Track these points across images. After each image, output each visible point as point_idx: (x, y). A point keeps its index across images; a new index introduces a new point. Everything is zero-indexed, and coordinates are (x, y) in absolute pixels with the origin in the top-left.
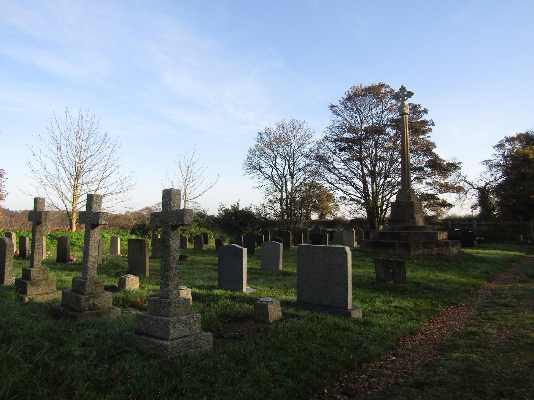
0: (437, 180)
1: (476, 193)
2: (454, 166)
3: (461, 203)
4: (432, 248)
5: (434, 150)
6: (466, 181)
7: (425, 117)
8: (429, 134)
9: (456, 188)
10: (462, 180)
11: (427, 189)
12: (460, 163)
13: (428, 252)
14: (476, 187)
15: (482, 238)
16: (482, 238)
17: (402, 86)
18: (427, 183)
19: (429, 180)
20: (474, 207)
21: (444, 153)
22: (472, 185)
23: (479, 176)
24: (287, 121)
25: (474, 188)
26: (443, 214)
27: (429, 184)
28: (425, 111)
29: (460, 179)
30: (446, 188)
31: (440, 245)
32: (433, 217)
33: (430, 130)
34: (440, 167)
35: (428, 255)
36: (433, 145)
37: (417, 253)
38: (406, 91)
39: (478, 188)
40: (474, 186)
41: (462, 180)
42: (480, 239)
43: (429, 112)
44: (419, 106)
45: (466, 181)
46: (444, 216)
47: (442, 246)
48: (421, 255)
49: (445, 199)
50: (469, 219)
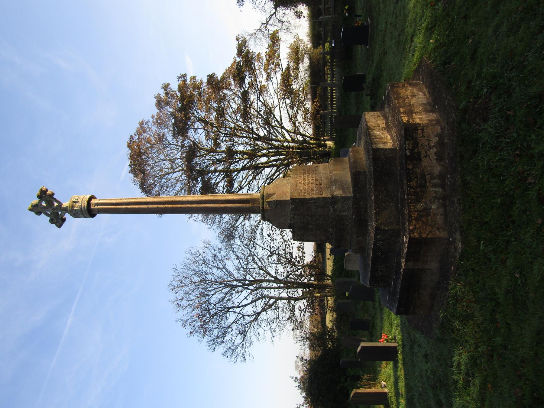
0: (262, 67)
1: (281, 10)
2: (242, 48)
3: (293, 28)
4: (423, 176)
5: (219, 76)
6: (267, 22)
7: (174, 87)
8: (198, 79)
9: (274, 43)
10: (266, 27)
11: (274, 80)
12: (237, 39)
13: (435, 186)
14: (274, 10)
15: (347, 7)
16: (347, 7)
17: (30, 210)
18: (267, 80)
19: (262, 78)
20: (299, 15)
21: (222, 62)
22: (272, 16)
23: (258, 10)
24: (172, 296)
25: (275, 13)
26: (307, 47)
27: (269, 76)
28: (166, 87)
29: (264, 30)
30: (273, 55)
31: (412, 151)
32: (310, 59)
33: (194, 78)
34: (245, 63)
35: (443, 186)
36: (211, 78)
37: (440, 219)
38: (40, 202)
39: (276, 8)
40: (272, 13)
41: (266, 27)
42: (348, 11)
43: (166, 82)
44: (158, 98)
45: (267, 22)
46: (309, 45)
47: (416, 144)
48: (444, 206)
49: (288, 46)
50: (314, 18)
